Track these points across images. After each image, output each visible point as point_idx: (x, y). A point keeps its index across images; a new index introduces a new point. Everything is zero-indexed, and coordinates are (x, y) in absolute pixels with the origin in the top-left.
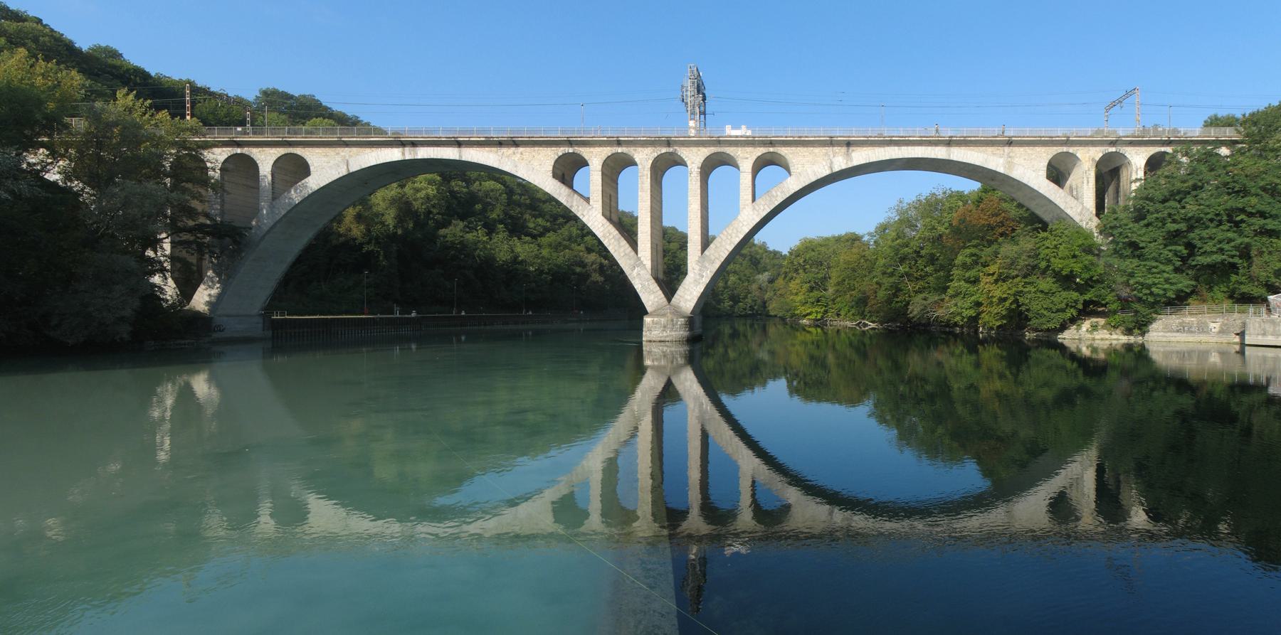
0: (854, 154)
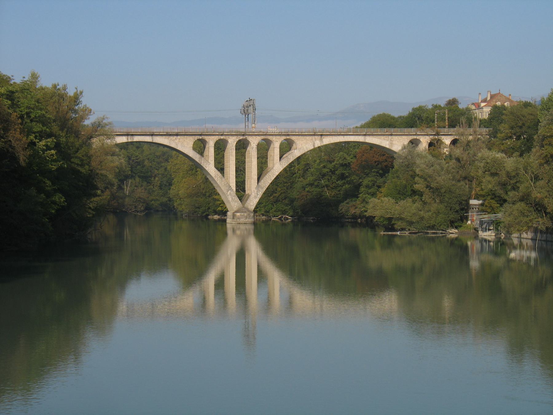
0: (324, 140)
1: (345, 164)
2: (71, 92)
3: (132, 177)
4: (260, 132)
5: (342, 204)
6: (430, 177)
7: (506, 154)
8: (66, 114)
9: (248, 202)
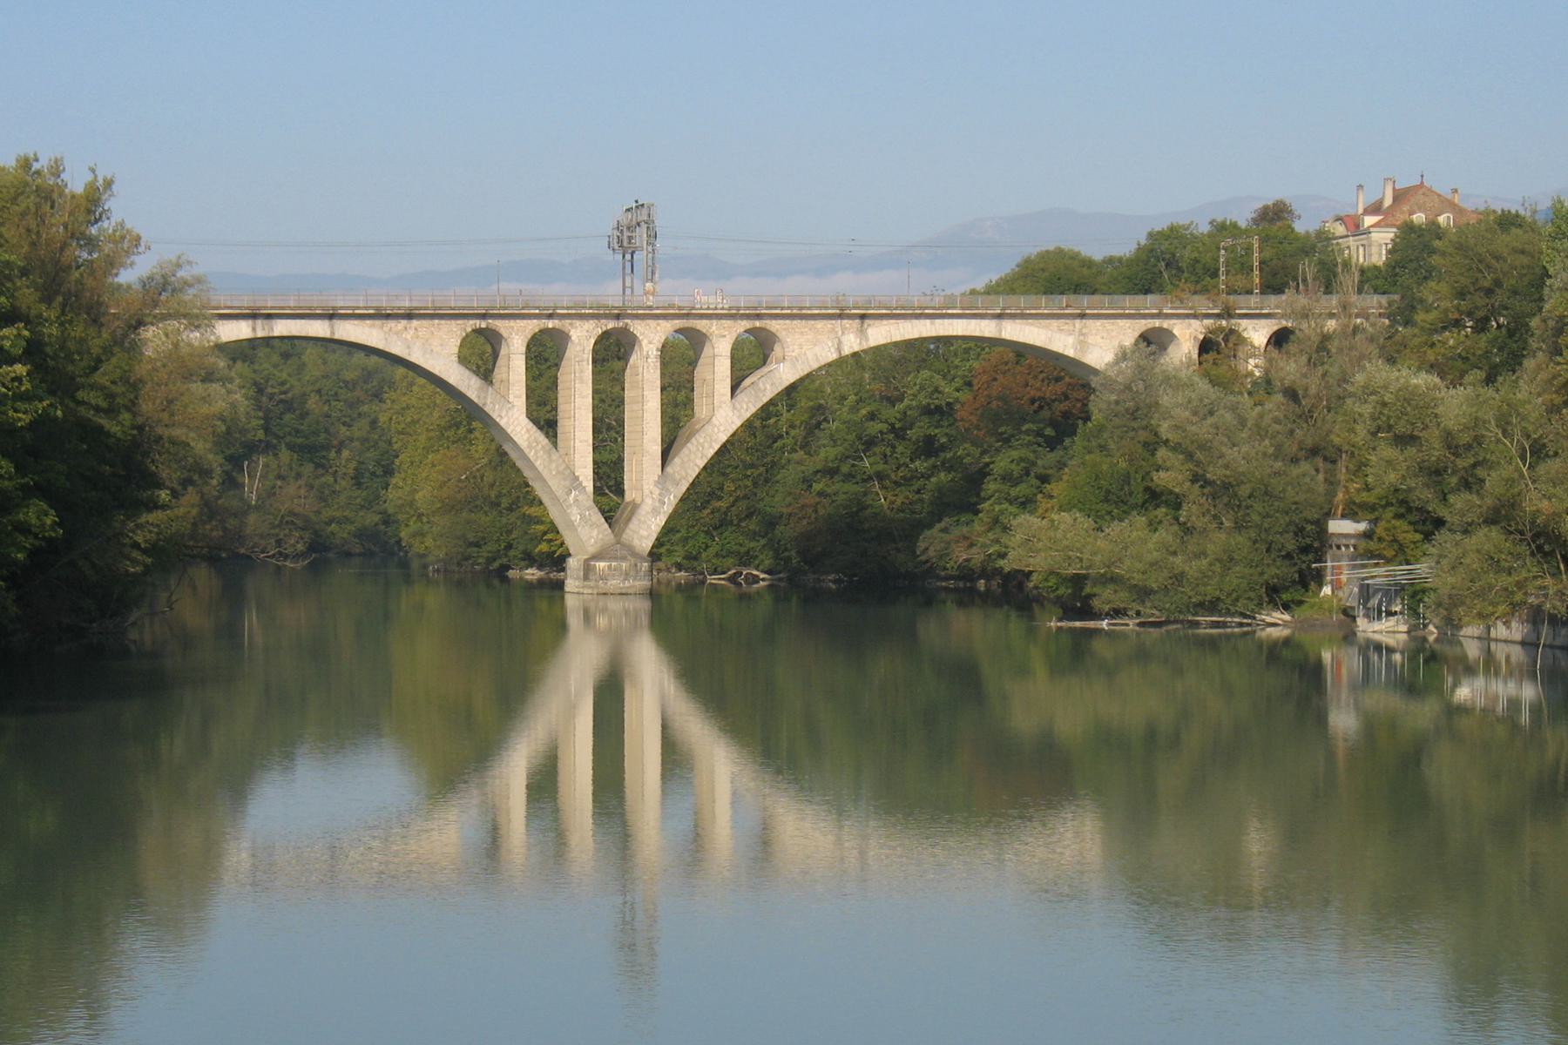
0: (870, 331)
1: (938, 409)
3: (268, 448)
4: (671, 306)
5: (928, 533)
6: (1202, 447)
9: (633, 525)
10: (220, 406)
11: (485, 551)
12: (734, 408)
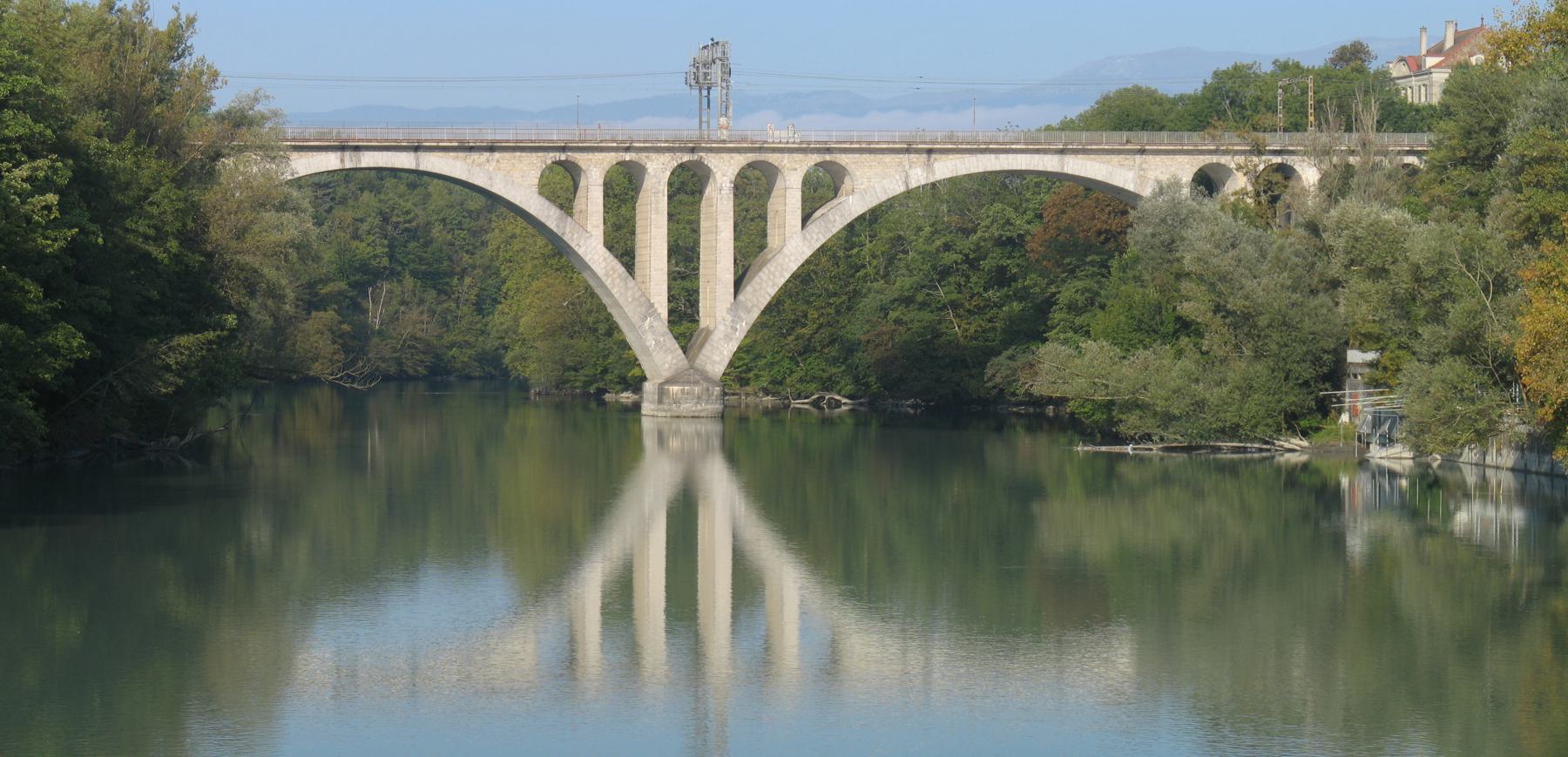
0: (936, 165)
1: (1010, 240)
2: (160, 20)
3: (393, 274)
4: (743, 140)
5: (996, 360)
6: (1223, 278)
7: (1414, 213)
8: (143, 84)
9: (707, 350)
10: (291, 233)
11: (581, 377)
12: (805, 238)
